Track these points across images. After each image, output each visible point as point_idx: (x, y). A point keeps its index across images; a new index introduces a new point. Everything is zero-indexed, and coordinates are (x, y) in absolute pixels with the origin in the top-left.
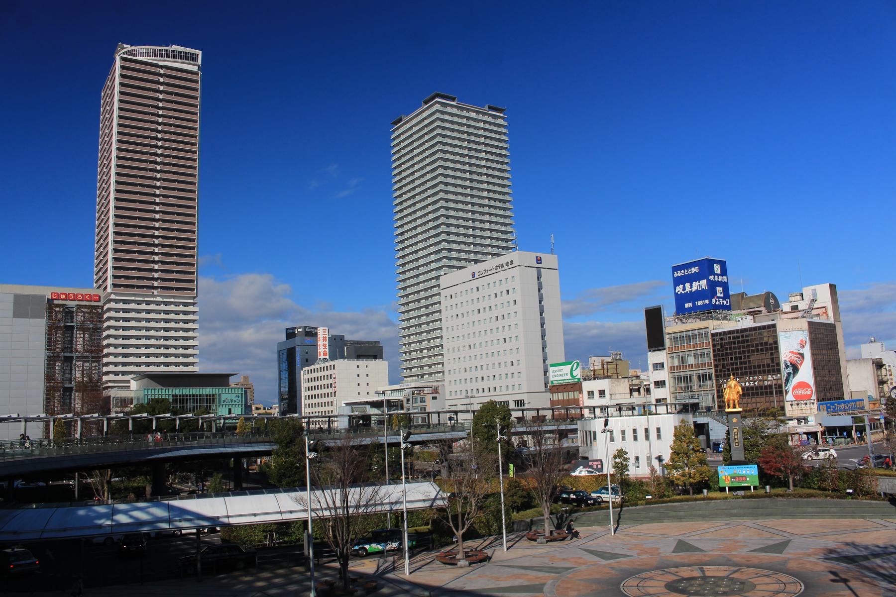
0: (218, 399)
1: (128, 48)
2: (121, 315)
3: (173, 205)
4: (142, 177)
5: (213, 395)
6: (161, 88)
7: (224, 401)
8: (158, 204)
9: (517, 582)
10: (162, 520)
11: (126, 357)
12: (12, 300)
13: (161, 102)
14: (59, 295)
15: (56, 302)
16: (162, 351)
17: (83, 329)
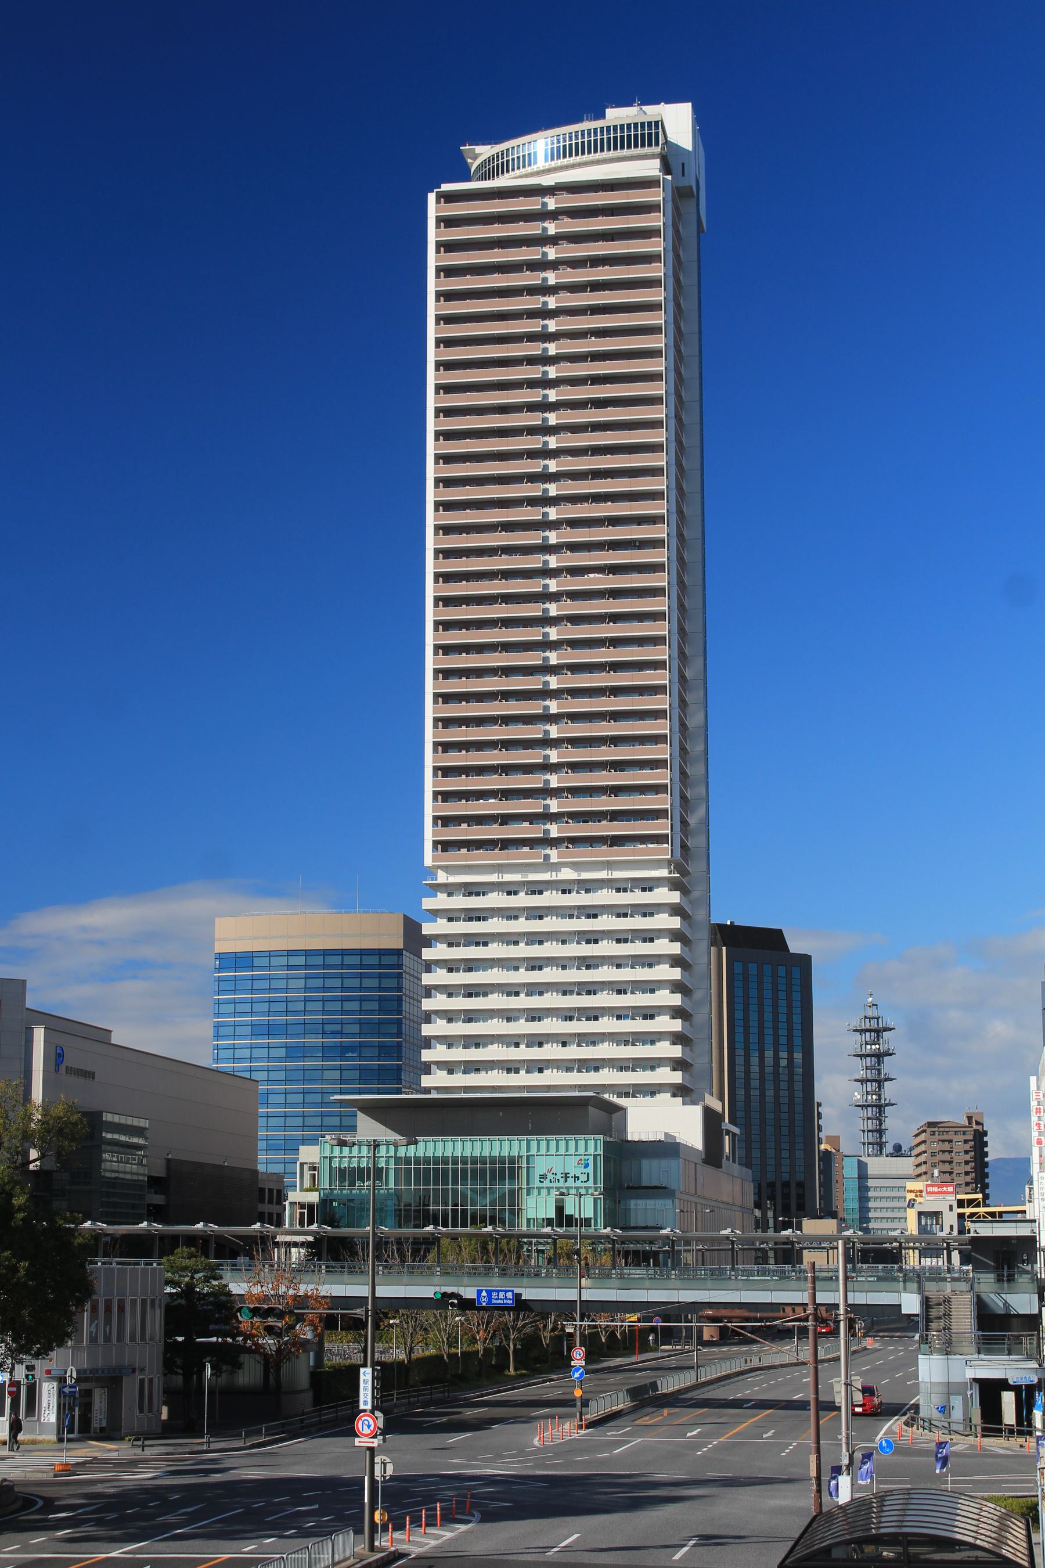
0: (524, 1171)
4: (508, 527)
7: (543, 1177)
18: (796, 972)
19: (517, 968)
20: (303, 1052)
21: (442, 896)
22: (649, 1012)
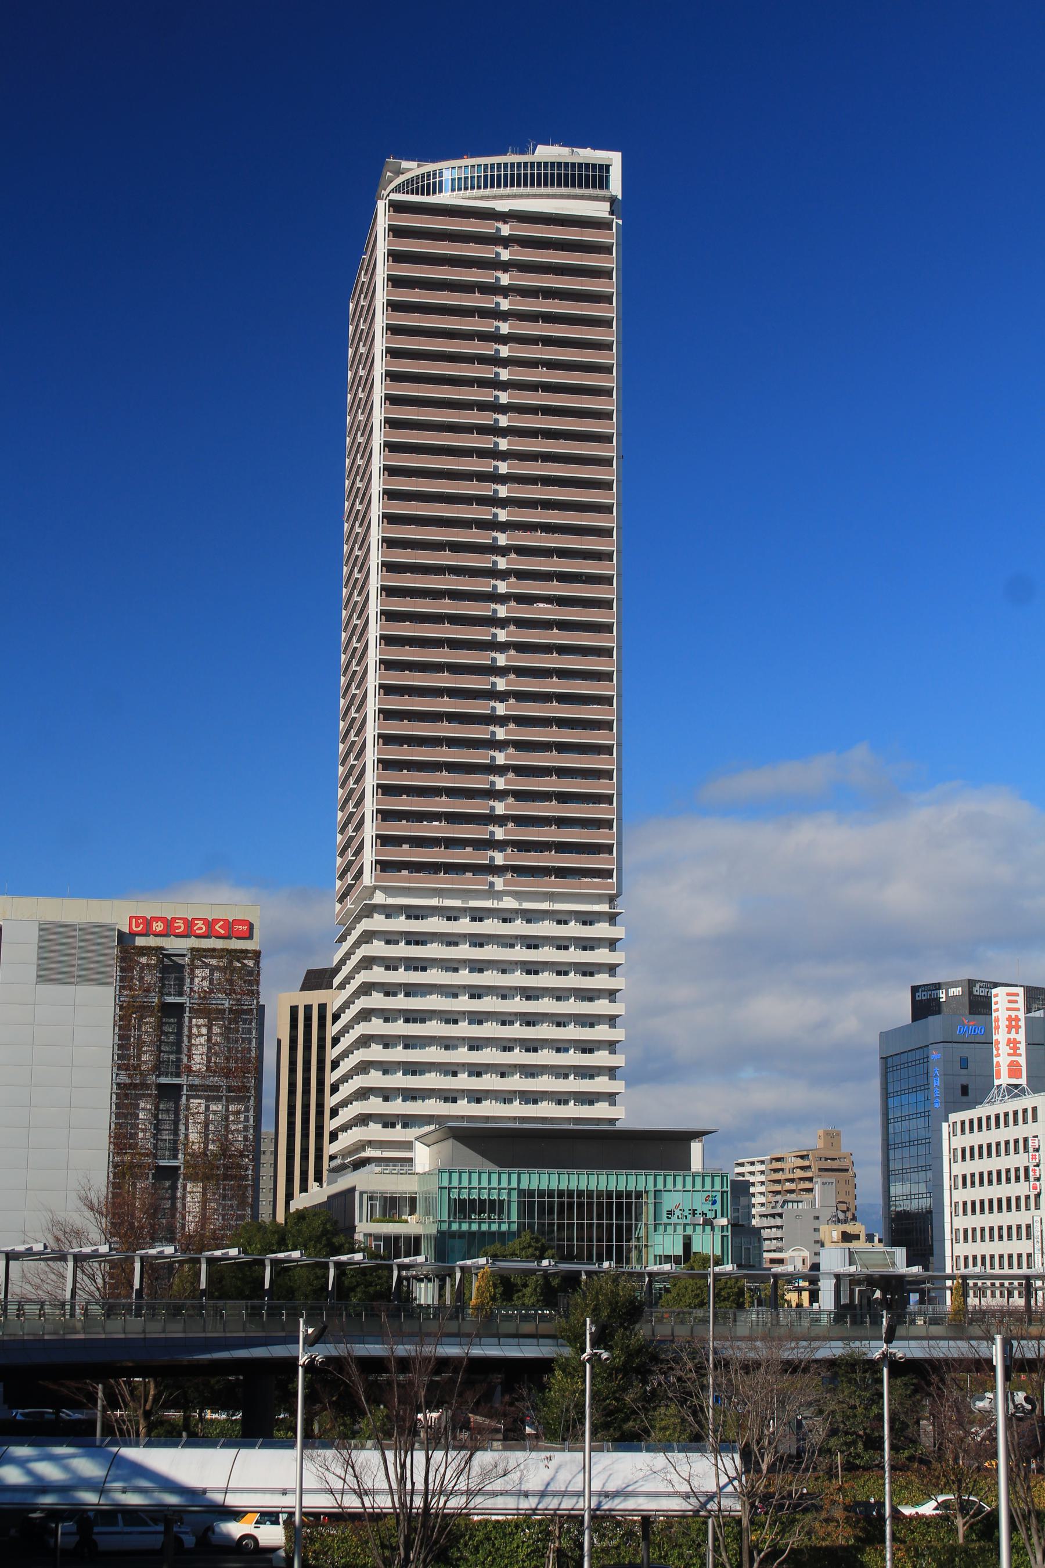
0: (651, 1207)
1: (412, 168)
2: (402, 950)
3: (547, 624)
6: (505, 279)
7: (671, 1213)
8: (503, 623)
10: (89, 1484)
11: (414, 1073)
12: (35, 938)
13: (505, 320)
14: (148, 922)
15: (140, 942)
16: (518, 1056)
17: (205, 1011)
22: (590, 1046)
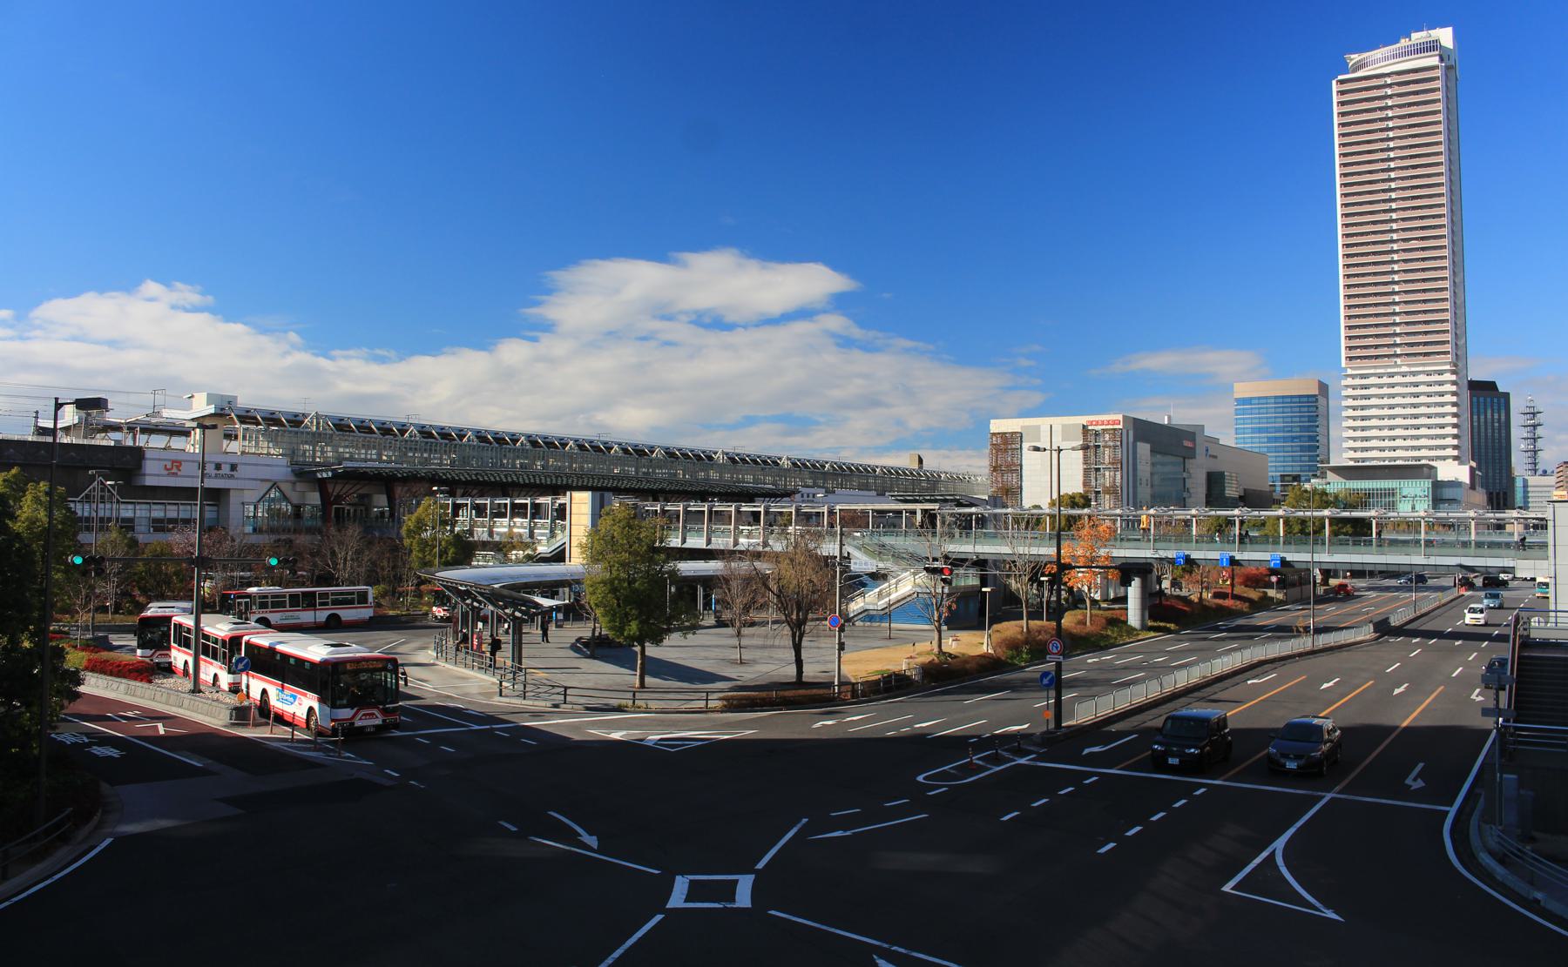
5: (1393, 489)
9: (1208, 689)
15: (1090, 428)
18: (1502, 400)
19: (1383, 408)
20: (1276, 439)
21: (1349, 379)
